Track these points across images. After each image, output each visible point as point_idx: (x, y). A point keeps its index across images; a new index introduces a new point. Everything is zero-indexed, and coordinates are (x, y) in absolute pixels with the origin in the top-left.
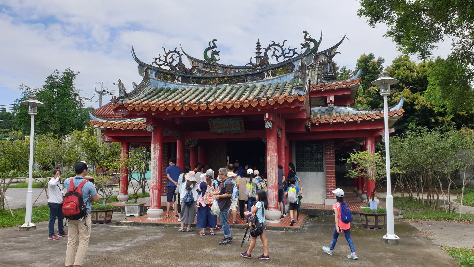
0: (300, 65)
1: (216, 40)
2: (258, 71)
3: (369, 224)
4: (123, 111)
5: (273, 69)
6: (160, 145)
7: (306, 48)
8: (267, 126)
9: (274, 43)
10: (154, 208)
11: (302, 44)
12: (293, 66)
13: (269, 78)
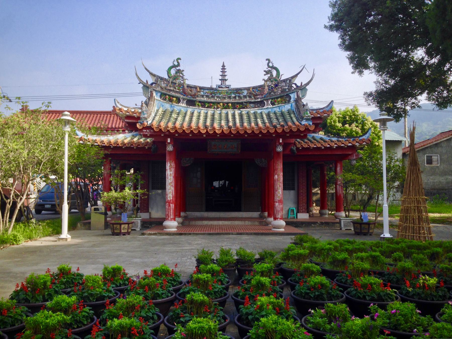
0: (296, 97)
1: (180, 59)
2: (259, 100)
4: (148, 131)
5: (272, 99)
6: (175, 163)
7: (269, 75)
10: (171, 220)
11: (265, 71)
12: (290, 98)
13: (269, 106)
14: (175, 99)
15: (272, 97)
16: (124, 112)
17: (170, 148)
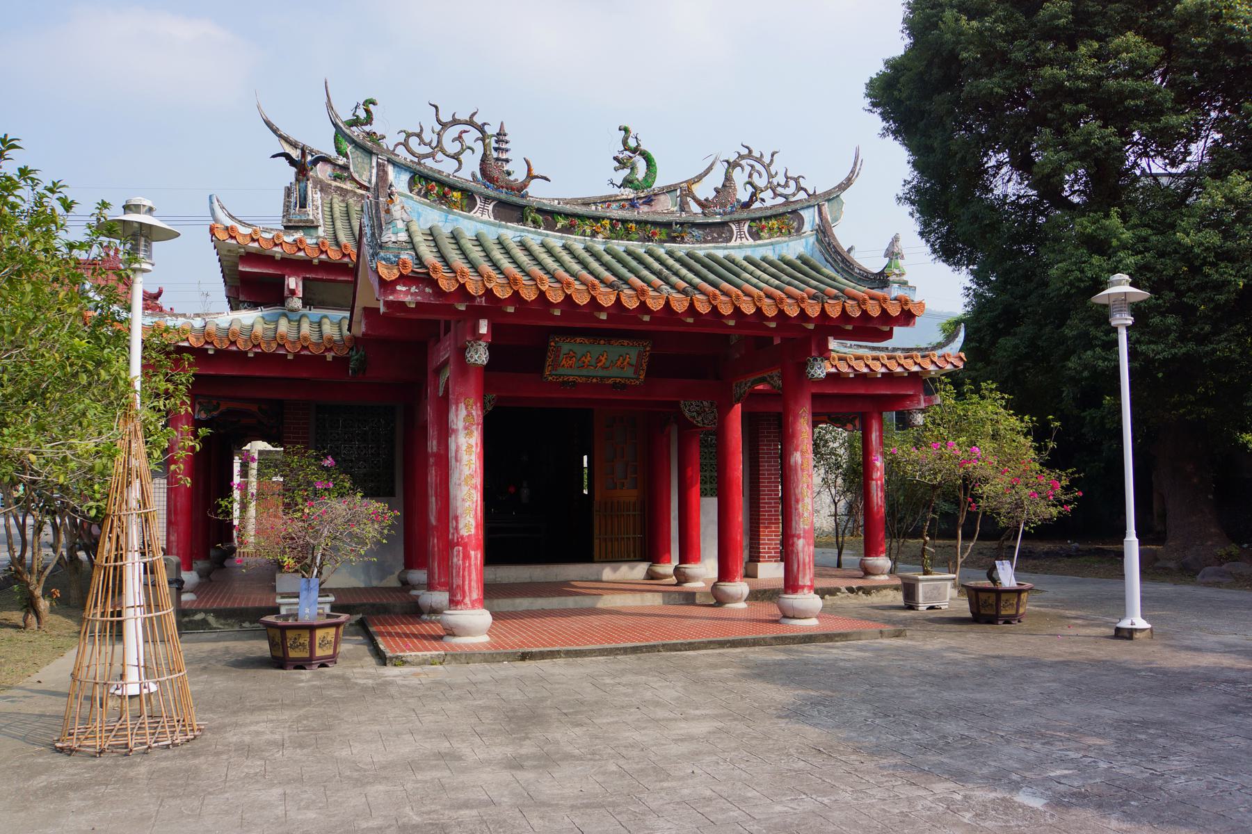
2: (718, 219)
3: (983, 612)
4: (413, 289)
7: (627, 171)
8: (819, 372)
9: (750, 151)
10: (473, 607)
14: (456, 195)
15: (754, 216)
16: (240, 240)
17: (480, 356)
